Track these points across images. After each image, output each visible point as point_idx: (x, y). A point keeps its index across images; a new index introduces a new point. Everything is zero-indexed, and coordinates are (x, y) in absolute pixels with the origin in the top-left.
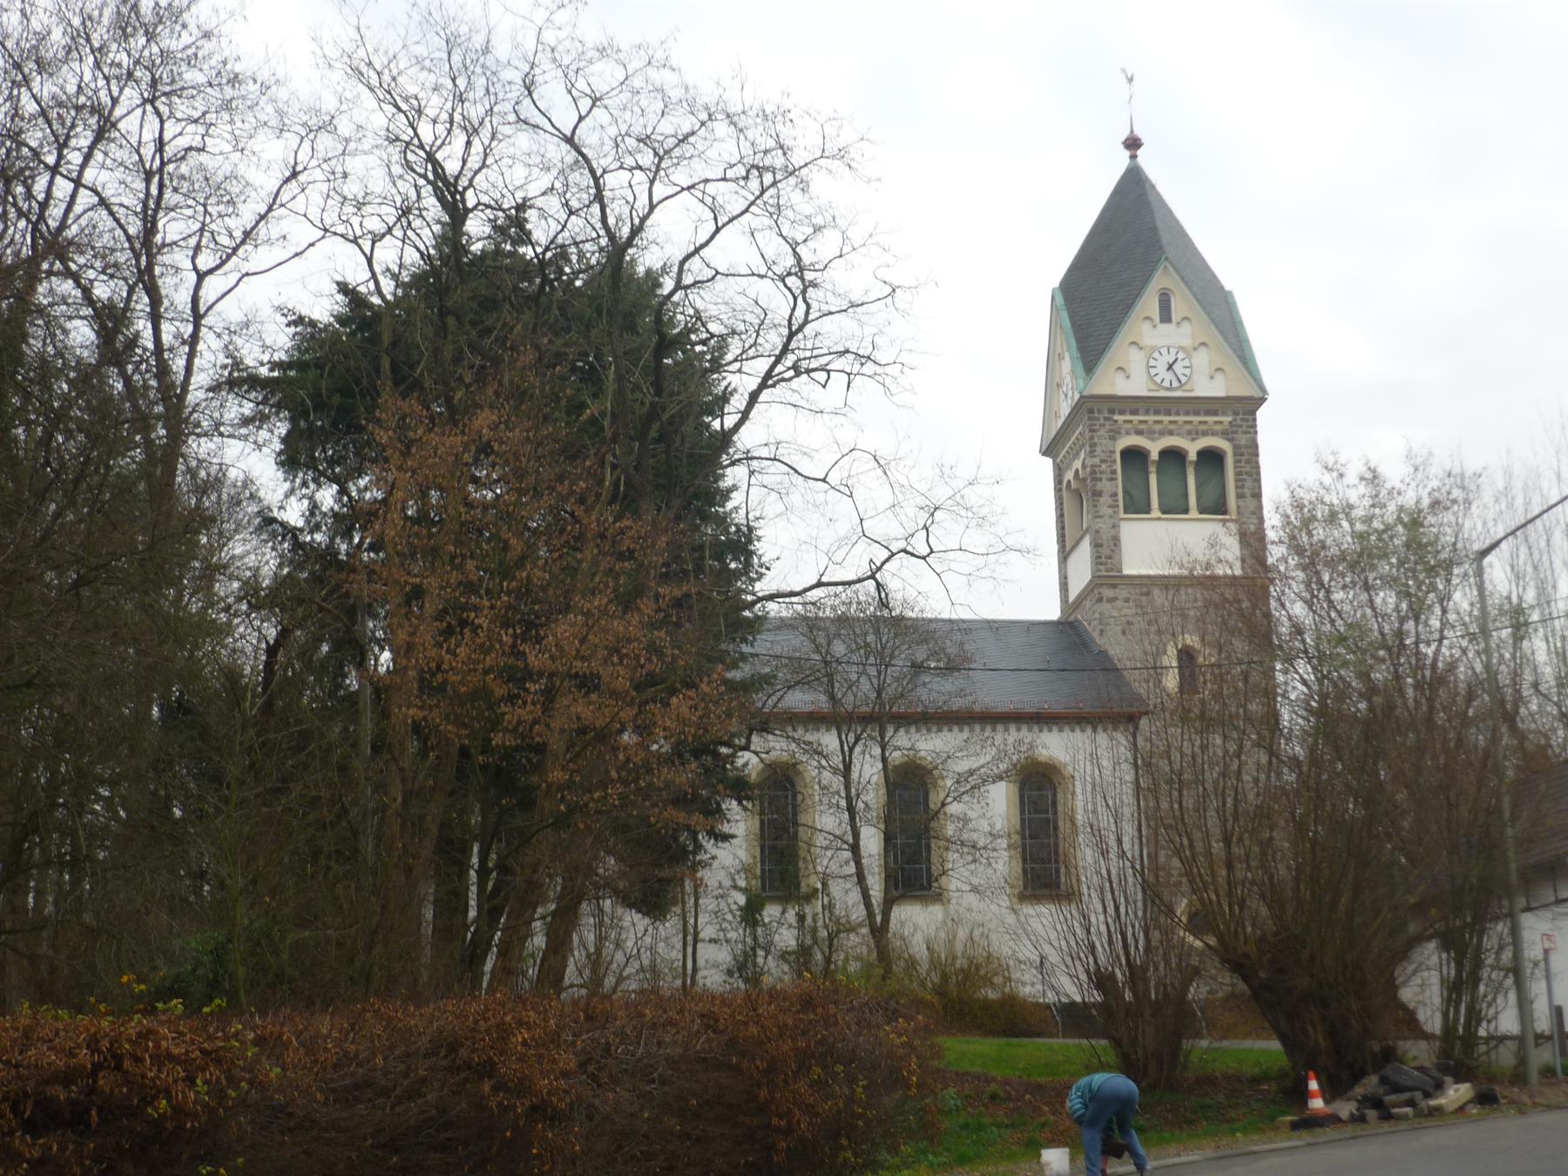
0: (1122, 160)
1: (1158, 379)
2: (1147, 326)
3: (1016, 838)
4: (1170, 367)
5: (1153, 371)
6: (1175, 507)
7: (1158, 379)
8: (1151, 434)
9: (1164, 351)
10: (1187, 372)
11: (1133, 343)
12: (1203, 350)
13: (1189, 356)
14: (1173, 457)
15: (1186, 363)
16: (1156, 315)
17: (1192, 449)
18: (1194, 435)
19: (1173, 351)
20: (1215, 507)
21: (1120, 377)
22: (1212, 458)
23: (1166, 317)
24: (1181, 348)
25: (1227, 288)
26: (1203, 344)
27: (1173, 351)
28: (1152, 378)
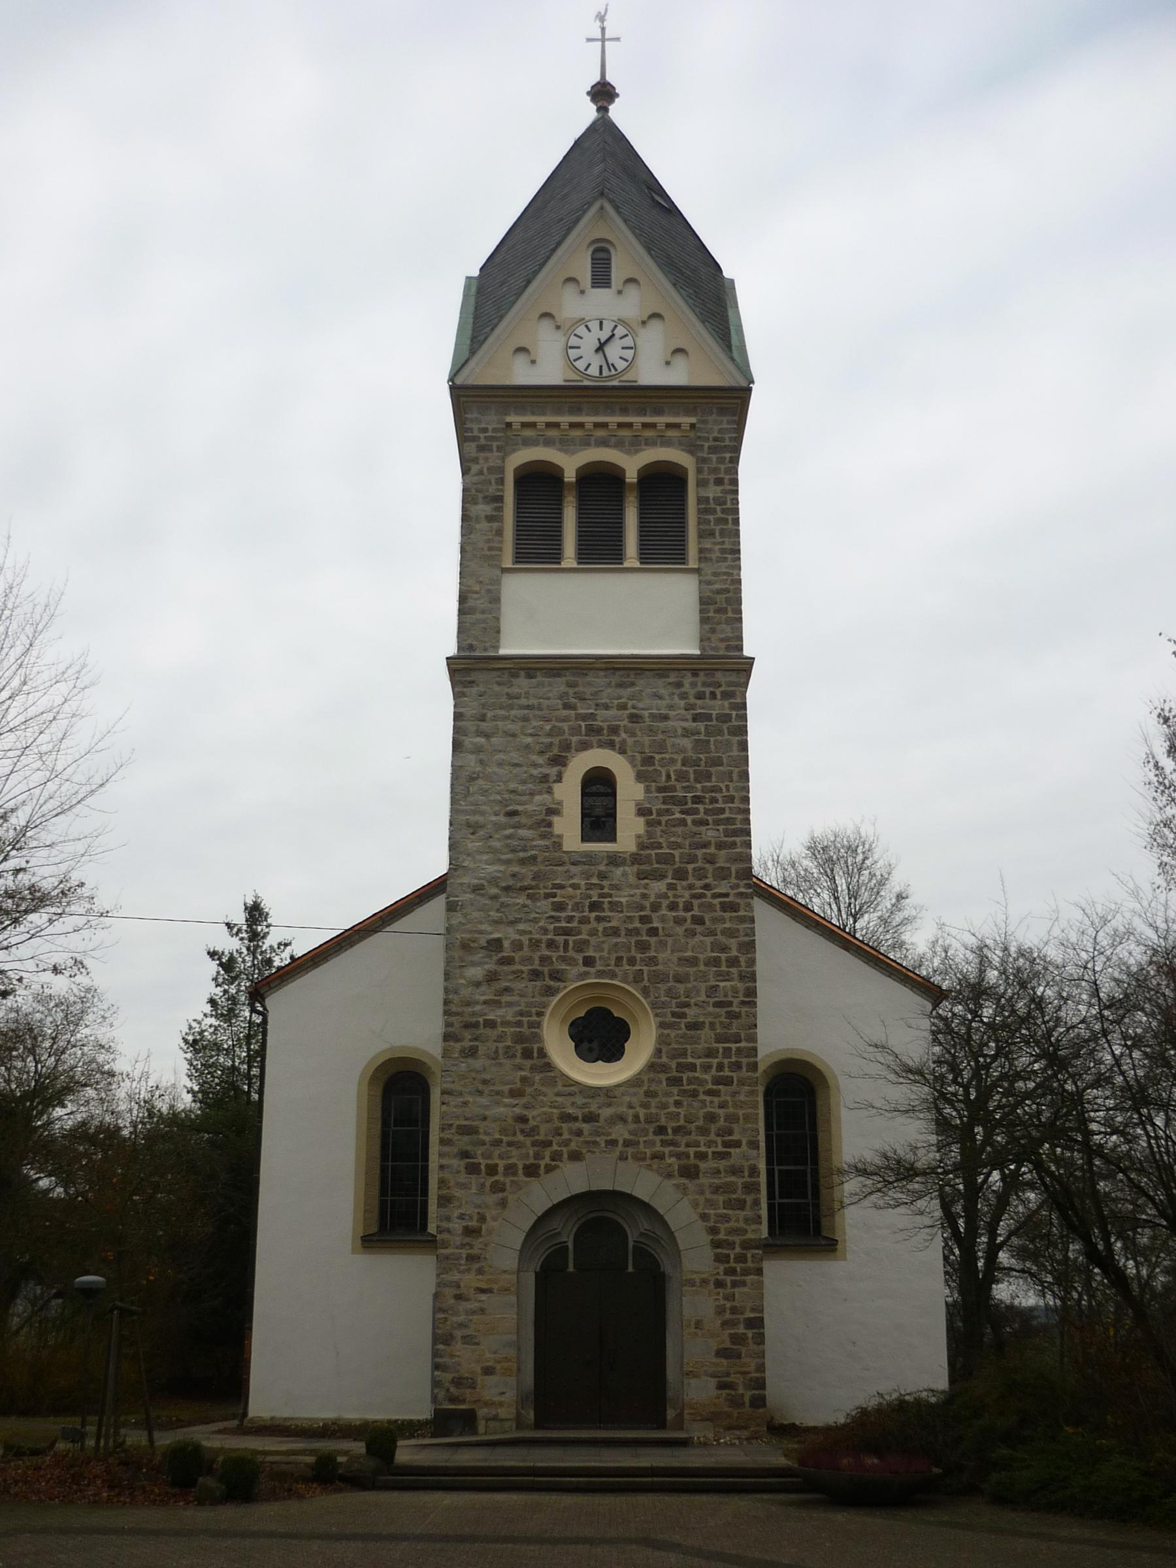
0: (588, 113)
1: (580, 365)
2: (570, 292)
3: (837, 1205)
4: (601, 348)
5: (573, 353)
6: (600, 550)
7: (580, 365)
8: (565, 444)
9: (594, 325)
10: (629, 354)
11: (547, 315)
12: (655, 325)
13: (631, 332)
14: (601, 483)
15: (628, 341)
16: (586, 276)
17: (631, 466)
18: (635, 445)
19: (608, 326)
20: (663, 549)
21: (521, 361)
22: (663, 484)
23: (601, 278)
24: (621, 321)
25: (727, 273)
26: (679, 351)
27: (608, 326)
28: (571, 363)
